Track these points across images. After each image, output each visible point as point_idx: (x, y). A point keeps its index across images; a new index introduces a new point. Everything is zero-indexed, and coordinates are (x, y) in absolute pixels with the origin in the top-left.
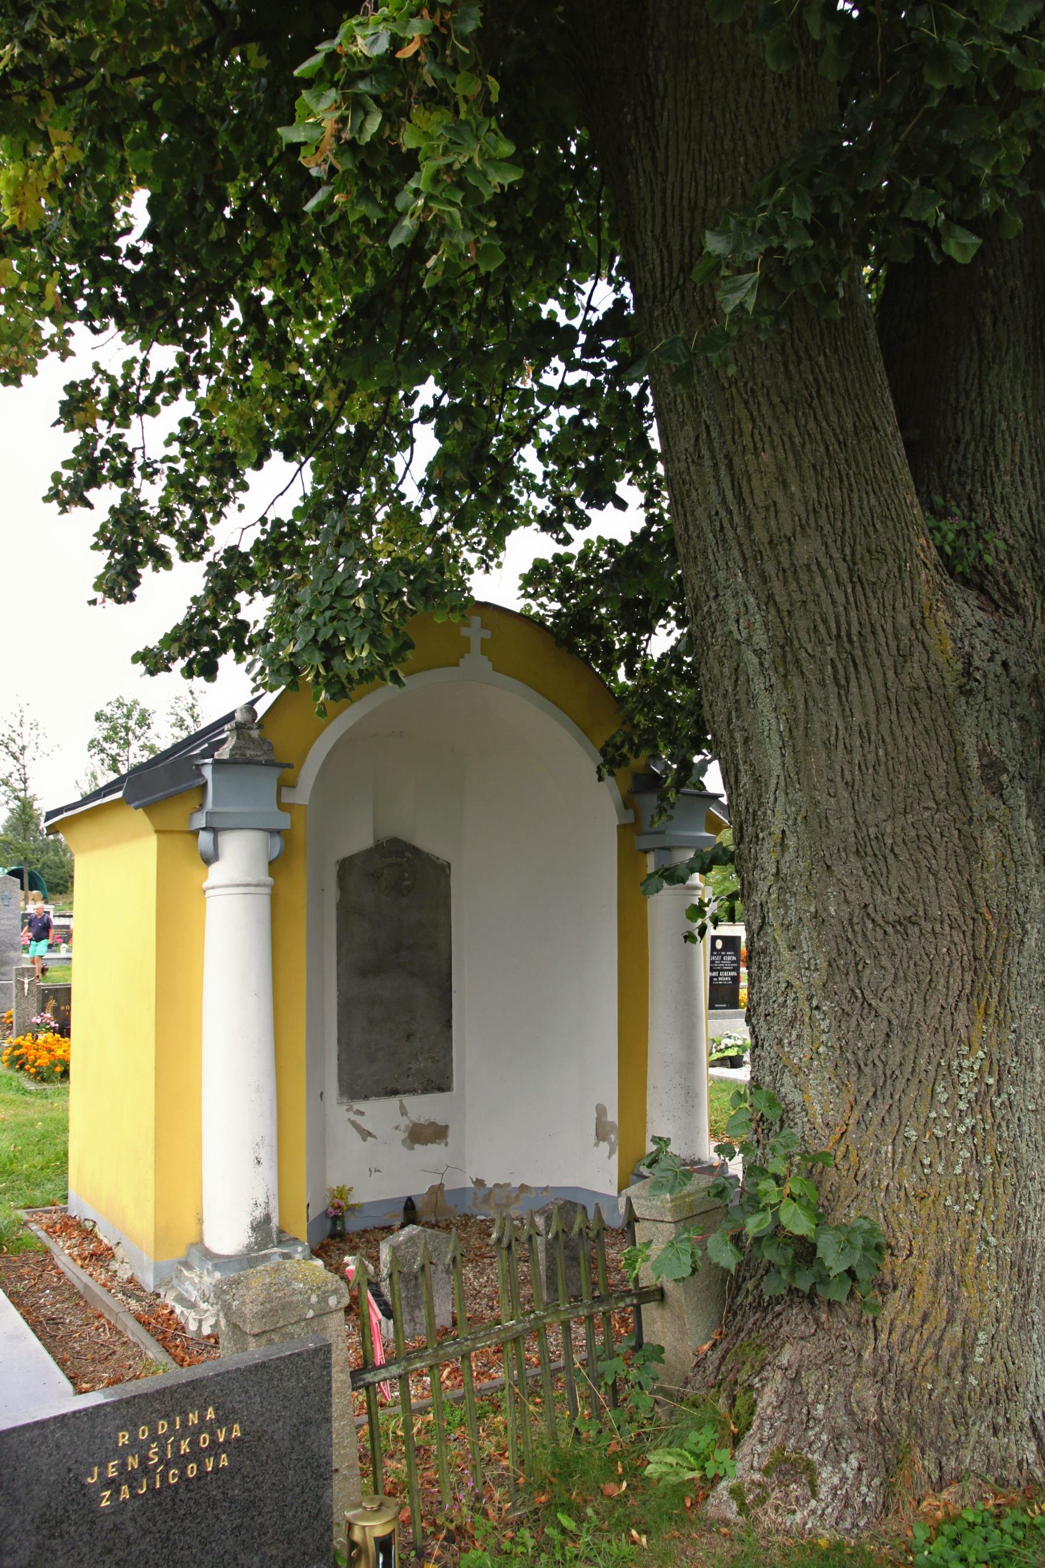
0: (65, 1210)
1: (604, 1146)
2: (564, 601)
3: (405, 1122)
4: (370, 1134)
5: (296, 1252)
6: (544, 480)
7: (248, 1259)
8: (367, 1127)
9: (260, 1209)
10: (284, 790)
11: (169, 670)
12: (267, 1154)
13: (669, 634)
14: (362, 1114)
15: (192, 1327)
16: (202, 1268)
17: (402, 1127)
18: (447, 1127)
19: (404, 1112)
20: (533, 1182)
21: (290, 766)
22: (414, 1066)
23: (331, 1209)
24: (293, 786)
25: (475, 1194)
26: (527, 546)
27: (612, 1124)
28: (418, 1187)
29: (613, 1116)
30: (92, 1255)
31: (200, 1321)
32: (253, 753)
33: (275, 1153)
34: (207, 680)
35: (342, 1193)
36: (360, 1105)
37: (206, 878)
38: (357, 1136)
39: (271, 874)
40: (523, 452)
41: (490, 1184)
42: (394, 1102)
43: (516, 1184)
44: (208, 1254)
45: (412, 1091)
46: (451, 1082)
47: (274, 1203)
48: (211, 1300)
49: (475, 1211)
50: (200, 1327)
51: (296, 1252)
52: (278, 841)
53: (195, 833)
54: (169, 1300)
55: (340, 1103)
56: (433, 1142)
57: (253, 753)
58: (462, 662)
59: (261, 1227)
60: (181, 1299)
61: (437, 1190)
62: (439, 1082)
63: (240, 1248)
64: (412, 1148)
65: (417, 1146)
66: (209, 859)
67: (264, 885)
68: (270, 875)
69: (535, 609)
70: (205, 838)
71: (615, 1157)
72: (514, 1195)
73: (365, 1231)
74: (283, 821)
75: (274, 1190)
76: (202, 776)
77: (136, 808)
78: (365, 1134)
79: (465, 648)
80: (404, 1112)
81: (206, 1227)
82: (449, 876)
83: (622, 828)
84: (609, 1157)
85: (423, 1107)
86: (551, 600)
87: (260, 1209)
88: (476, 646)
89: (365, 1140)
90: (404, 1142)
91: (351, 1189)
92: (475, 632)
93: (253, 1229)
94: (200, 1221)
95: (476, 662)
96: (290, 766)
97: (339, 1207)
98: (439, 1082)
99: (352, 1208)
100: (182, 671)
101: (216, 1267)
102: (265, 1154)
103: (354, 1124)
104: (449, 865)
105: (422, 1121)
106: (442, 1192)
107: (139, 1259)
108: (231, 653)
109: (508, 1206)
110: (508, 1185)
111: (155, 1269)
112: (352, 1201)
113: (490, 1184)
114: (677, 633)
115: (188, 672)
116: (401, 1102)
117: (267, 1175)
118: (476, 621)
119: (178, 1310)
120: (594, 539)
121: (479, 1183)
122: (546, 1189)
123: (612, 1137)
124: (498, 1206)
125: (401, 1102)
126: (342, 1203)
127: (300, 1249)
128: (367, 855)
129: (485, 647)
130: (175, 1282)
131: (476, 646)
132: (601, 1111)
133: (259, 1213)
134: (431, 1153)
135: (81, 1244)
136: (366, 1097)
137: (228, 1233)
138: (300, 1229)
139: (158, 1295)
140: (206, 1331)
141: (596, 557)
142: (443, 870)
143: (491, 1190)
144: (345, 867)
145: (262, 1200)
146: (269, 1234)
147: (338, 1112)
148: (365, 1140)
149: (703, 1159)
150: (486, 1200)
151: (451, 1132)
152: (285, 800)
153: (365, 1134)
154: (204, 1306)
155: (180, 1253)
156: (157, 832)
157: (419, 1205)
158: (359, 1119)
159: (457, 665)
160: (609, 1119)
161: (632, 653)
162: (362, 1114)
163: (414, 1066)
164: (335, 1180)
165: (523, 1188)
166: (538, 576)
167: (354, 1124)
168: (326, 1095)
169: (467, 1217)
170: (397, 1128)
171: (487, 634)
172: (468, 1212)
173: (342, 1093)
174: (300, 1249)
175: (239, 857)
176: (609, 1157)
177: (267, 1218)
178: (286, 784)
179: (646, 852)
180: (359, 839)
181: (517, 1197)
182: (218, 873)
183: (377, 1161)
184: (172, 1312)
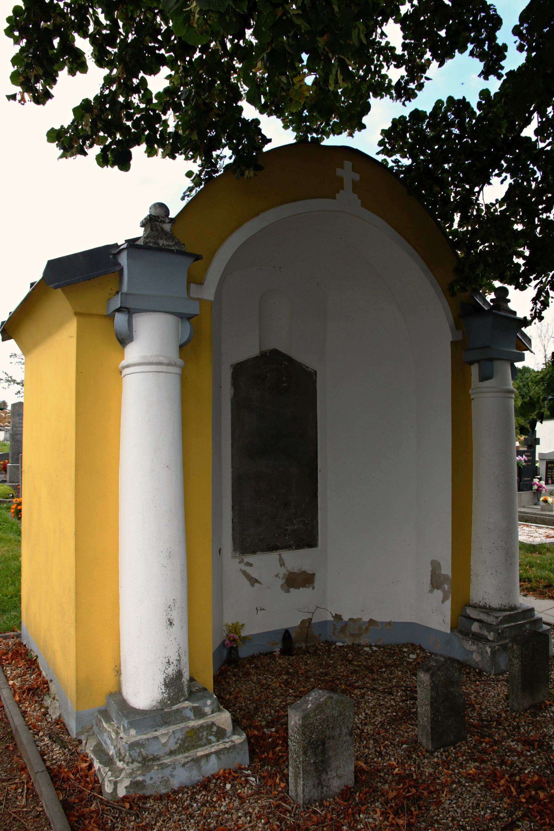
0: (19, 636)
1: (439, 594)
2: (414, 158)
3: (283, 571)
4: (257, 581)
5: (206, 705)
6: (403, 50)
7: (160, 716)
8: (255, 575)
9: (172, 667)
10: (192, 285)
11: (85, 154)
12: (178, 616)
13: (502, 182)
14: (251, 565)
15: (108, 789)
16: (119, 722)
17: (281, 575)
18: (314, 575)
19: (282, 564)
20: (379, 618)
21: (197, 258)
22: (290, 528)
23: (227, 642)
24: (201, 283)
25: (334, 625)
26: (382, 113)
27: (445, 576)
28: (292, 621)
29: (446, 569)
30: (29, 690)
31: (116, 783)
32: (165, 243)
33: (186, 613)
34: (121, 169)
35: (235, 628)
36: (249, 558)
37: (123, 358)
38: (247, 583)
39: (181, 356)
40: (386, 28)
41: (346, 618)
42: (273, 557)
43: (366, 619)
44: (126, 709)
45: (288, 547)
46: (317, 540)
47: (185, 659)
48: (126, 759)
49: (334, 638)
50: (115, 789)
51: (206, 705)
52: (187, 325)
53: (111, 317)
54: (89, 749)
55: (234, 557)
56: (304, 586)
57: (165, 243)
58: (337, 195)
59: (173, 683)
60: (100, 751)
61: (307, 624)
62: (307, 539)
63: (154, 703)
64: (289, 592)
65: (292, 590)
66: (124, 340)
67: (175, 365)
68: (181, 357)
69: (391, 164)
70: (120, 319)
71: (448, 603)
72: (364, 627)
73: (253, 657)
74: (193, 309)
75: (185, 647)
76: (119, 265)
77: (56, 288)
78: (253, 581)
79: (339, 185)
80: (282, 564)
81: (123, 678)
82: (315, 382)
83: (454, 344)
84: (443, 602)
85: (297, 559)
86: (404, 156)
87: (172, 667)
88: (348, 185)
89: (253, 585)
90: (282, 587)
91: (243, 625)
92: (347, 173)
93: (166, 685)
94: (118, 673)
95: (348, 199)
96: (197, 258)
97: (234, 640)
98: (307, 539)
99: (244, 639)
100: (98, 158)
101: (132, 725)
102: (175, 616)
103: (245, 573)
104: (316, 372)
105: (296, 570)
106: (310, 623)
107: (66, 702)
108: (144, 146)
109: (359, 635)
110: (360, 619)
111: (77, 718)
112: (244, 633)
113: (346, 618)
114: (509, 181)
115: (103, 160)
116: (280, 555)
117: (179, 632)
118: (348, 164)
119: (97, 765)
120: (445, 100)
121: (338, 617)
122: (389, 623)
123: (446, 587)
124: (352, 635)
125: (280, 555)
126: (237, 637)
127: (209, 702)
128: (255, 360)
129: (356, 187)
130: (95, 729)
131: (348, 185)
132: (435, 566)
133: (171, 671)
134: (302, 594)
135: (25, 674)
136: (254, 552)
137: (143, 689)
138: (207, 678)
139: (80, 742)
140: (122, 792)
141: (445, 117)
142: (310, 377)
143: (346, 623)
144: (239, 370)
145: (174, 658)
146: (181, 690)
147: (232, 564)
148: (253, 585)
149: (518, 605)
150: (343, 630)
151: (317, 578)
152: (193, 294)
153: (253, 581)
154: (120, 764)
155: (100, 702)
156: (77, 314)
157: (293, 635)
158: (248, 570)
159: (334, 198)
160: (443, 572)
161: (467, 202)
162: (251, 565)
163: (290, 528)
164: (229, 619)
165: (372, 622)
166: (394, 136)
167: (245, 573)
168: (223, 551)
169: (329, 643)
170: (277, 576)
171: (357, 177)
172: (329, 639)
173: (235, 550)
174: (209, 702)
175: (151, 337)
176: (443, 602)
177: (179, 674)
178: (195, 280)
179: (471, 363)
180: (249, 350)
181: (367, 629)
182: (133, 353)
183: (266, 607)
184: (91, 766)
